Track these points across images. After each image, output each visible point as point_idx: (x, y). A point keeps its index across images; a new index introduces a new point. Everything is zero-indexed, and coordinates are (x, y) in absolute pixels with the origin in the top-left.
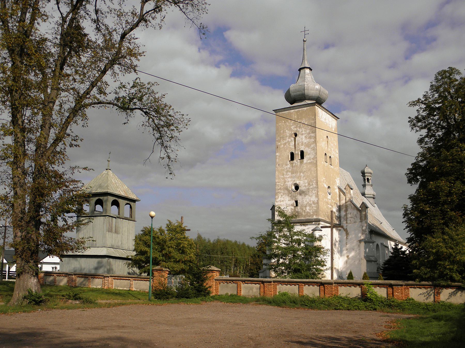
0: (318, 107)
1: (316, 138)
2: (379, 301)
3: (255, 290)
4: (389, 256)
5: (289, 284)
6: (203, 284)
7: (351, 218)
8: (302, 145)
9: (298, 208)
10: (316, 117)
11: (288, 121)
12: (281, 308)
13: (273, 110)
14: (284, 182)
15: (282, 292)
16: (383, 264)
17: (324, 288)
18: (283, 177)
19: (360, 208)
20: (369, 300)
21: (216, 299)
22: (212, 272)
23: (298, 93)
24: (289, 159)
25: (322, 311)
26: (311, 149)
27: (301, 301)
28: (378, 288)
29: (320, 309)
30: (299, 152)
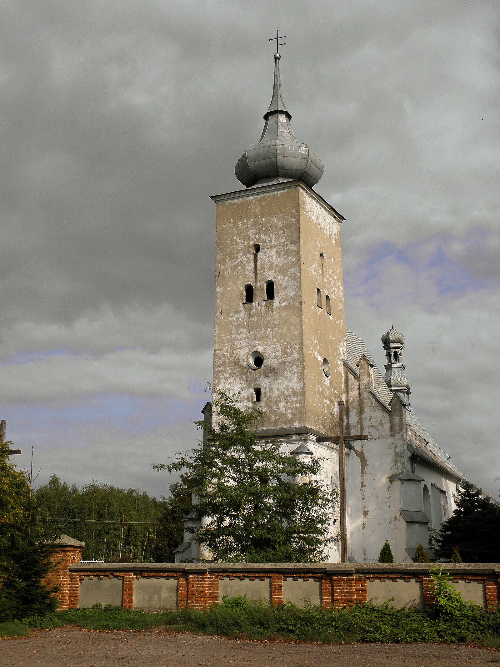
0: (304, 190)
1: (299, 255)
2: (468, 616)
3: (165, 594)
4: (454, 512)
5: (247, 577)
6: (39, 582)
7: (371, 428)
8: (271, 268)
9: (262, 406)
10: (301, 210)
11: (241, 221)
12: (231, 641)
13: (211, 197)
14: (231, 348)
15: (230, 597)
16: (441, 528)
17: (332, 586)
18: (229, 337)
19: (390, 408)
20: (443, 614)
21: (70, 621)
22: (64, 551)
23: (263, 162)
24: (242, 299)
25: (334, 648)
26: (289, 277)
27: (279, 620)
28: (461, 582)
29: (327, 641)
30: (263, 285)
